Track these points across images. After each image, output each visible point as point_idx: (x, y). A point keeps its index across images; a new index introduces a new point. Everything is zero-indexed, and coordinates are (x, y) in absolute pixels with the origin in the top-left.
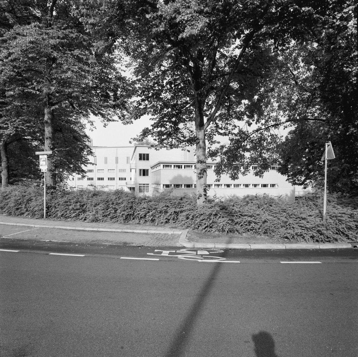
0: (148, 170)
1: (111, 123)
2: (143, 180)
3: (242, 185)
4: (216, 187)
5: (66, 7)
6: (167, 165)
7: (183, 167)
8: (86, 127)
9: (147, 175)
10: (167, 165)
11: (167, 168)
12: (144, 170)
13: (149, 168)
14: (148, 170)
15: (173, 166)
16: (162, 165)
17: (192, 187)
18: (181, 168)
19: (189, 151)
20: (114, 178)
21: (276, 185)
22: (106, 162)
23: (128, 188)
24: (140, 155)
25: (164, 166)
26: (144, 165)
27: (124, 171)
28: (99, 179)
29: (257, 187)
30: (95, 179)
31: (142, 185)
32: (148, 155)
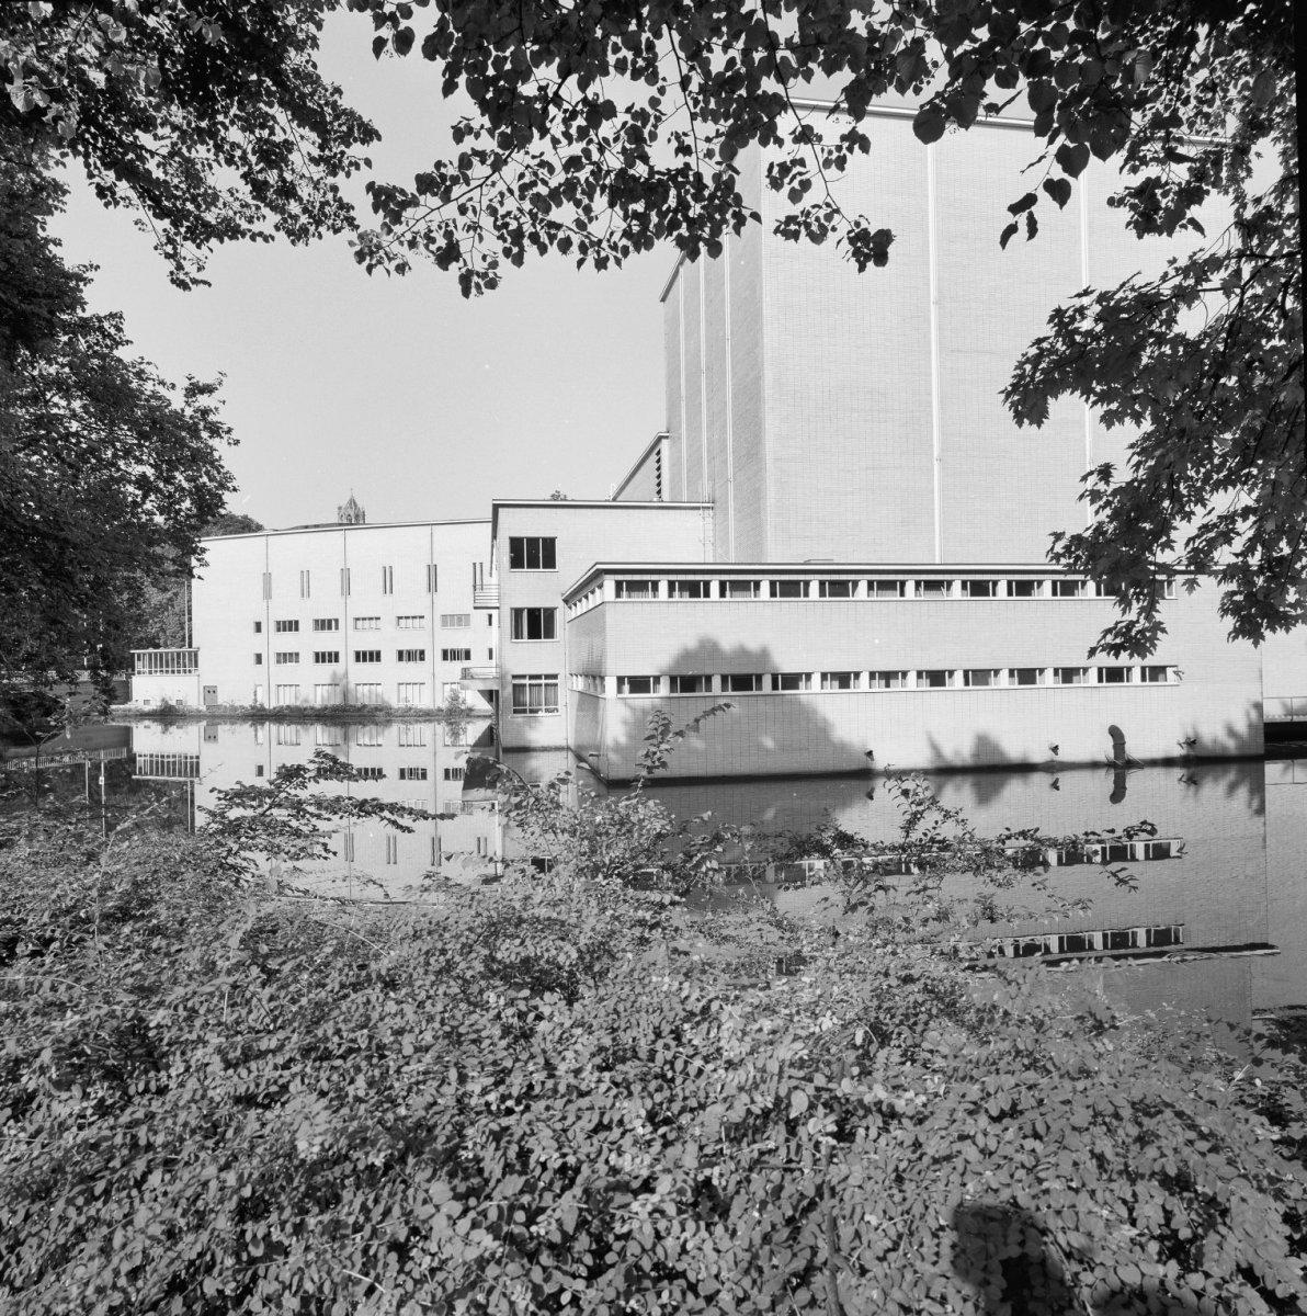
0: (550, 613)
1: (221, 252)
2: (531, 657)
3: (1004, 674)
4: (879, 685)
5: (803, 879)
6: (635, 582)
7: (715, 588)
8: (128, 334)
9: (550, 634)
10: (635, 582)
11: (637, 597)
12: (534, 613)
13: (553, 601)
14: (550, 613)
15: (663, 587)
16: (609, 583)
17: (759, 688)
18: (707, 594)
19: (872, 247)
20: (422, 652)
21: (1169, 671)
22: (388, 586)
23: (481, 692)
24: (516, 543)
25: (619, 584)
26: (534, 588)
27: (461, 620)
28: (361, 657)
29: (1078, 682)
30: (347, 658)
31: (527, 681)
32: (550, 543)
